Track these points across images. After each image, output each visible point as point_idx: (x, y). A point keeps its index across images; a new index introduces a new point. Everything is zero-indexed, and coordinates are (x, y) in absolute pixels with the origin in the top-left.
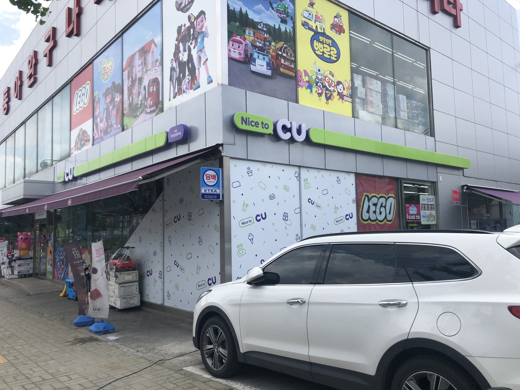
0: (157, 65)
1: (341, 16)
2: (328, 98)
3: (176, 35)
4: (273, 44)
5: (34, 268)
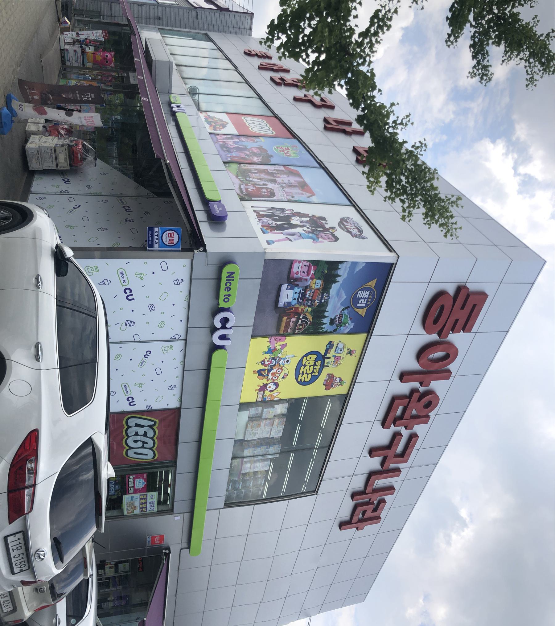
0: (288, 197)
1: (342, 386)
2: (260, 373)
3: (318, 215)
4: (310, 309)
5: (72, 67)
